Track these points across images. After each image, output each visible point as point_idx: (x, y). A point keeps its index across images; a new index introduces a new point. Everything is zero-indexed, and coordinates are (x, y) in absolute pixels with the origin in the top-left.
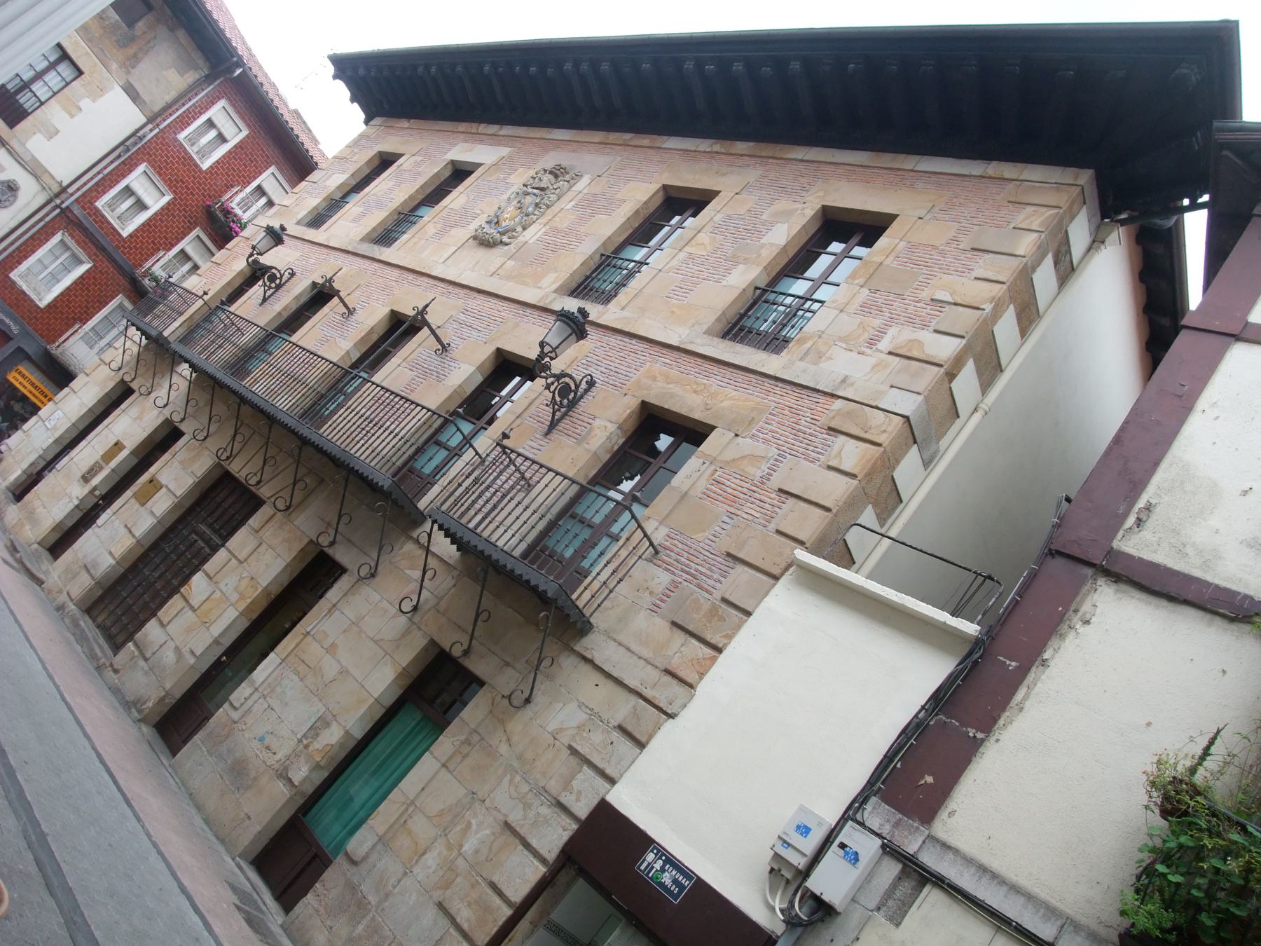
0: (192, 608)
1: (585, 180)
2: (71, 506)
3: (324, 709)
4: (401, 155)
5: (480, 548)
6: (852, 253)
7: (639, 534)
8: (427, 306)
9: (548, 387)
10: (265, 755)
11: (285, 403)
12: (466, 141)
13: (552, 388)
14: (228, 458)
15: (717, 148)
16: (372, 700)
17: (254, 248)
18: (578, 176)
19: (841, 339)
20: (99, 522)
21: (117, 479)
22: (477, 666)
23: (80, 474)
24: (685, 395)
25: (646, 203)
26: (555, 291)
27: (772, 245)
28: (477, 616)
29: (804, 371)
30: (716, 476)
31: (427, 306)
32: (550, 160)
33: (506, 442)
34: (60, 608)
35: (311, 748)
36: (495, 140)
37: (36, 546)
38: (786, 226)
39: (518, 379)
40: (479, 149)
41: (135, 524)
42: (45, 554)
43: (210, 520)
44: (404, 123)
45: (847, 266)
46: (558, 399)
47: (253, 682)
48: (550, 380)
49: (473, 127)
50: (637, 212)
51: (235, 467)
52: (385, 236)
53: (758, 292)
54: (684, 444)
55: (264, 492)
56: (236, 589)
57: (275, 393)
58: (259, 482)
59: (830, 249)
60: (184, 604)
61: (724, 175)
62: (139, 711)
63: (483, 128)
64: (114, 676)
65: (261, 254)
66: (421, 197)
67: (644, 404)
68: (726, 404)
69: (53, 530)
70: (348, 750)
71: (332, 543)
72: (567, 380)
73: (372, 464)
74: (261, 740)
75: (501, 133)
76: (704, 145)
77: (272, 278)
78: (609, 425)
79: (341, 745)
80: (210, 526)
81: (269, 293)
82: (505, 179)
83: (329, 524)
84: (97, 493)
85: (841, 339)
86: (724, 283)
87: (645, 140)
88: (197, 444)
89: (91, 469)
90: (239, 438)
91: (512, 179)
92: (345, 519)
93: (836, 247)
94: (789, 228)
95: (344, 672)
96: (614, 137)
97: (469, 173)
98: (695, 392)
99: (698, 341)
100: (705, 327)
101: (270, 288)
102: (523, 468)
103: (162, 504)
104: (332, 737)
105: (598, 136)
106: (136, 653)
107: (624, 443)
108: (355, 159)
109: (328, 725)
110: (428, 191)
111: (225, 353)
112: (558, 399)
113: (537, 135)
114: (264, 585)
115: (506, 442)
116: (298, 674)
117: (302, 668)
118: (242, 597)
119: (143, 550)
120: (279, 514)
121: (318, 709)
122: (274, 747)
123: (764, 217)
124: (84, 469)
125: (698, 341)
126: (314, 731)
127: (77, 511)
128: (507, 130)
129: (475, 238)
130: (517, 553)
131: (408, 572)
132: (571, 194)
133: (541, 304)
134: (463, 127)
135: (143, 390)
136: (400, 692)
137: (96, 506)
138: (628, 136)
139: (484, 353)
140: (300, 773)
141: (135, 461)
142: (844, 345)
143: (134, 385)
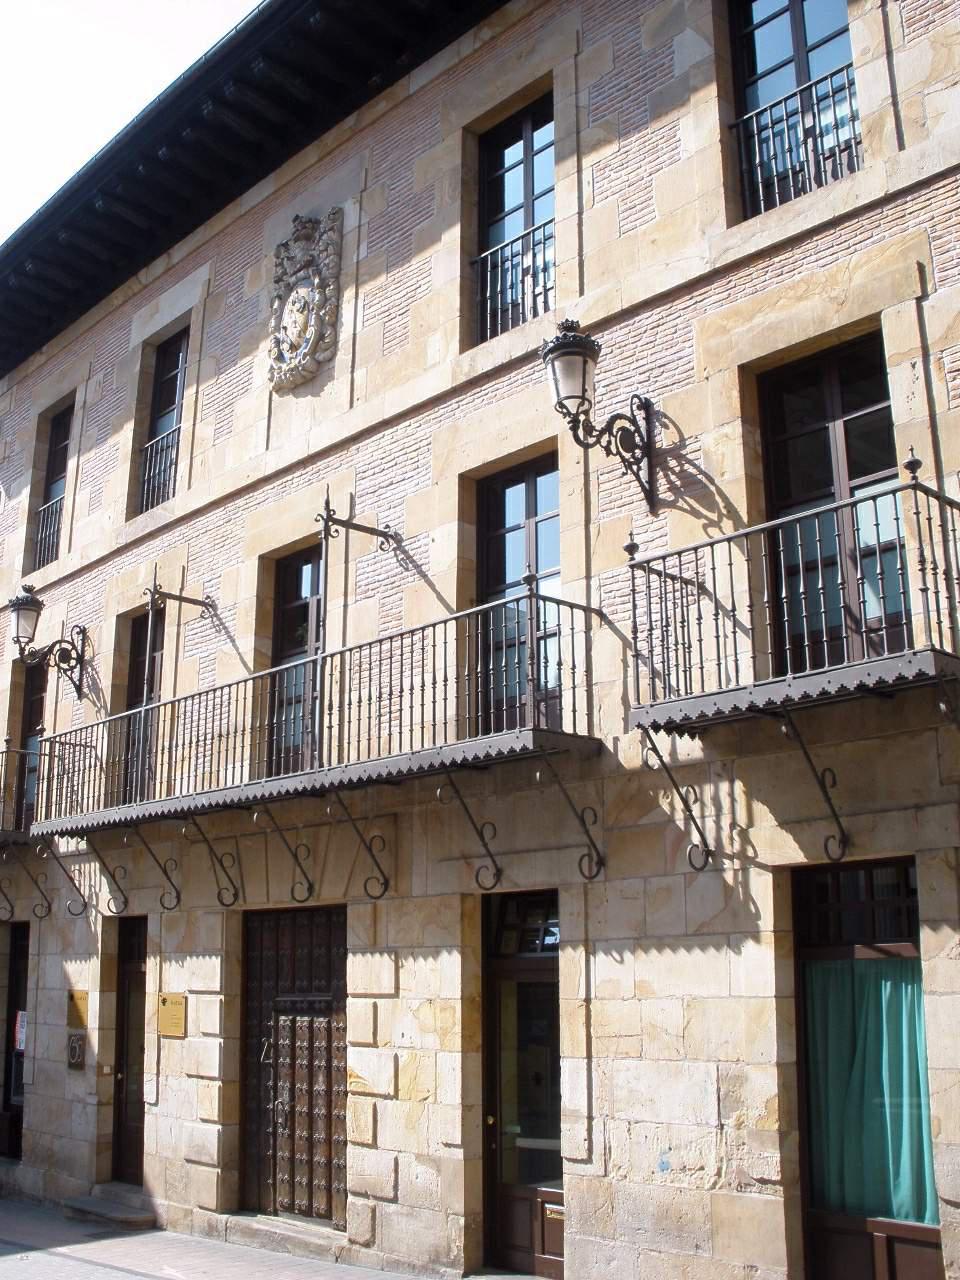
0: (386, 1097)
1: (351, 210)
2: (92, 1110)
3: (713, 1067)
4: (73, 394)
5: (761, 703)
6: (537, 147)
7: (565, 609)
8: (327, 503)
9: (608, 452)
10: (686, 1181)
11: (236, 776)
12: (139, 307)
13: (613, 449)
14: (236, 896)
15: (486, 33)
16: (774, 999)
17: (18, 641)
18: (338, 214)
19: (926, 83)
20: (149, 1094)
21: (113, 1034)
22: (882, 843)
23: (63, 1067)
24: (796, 309)
25: (463, 165)
26: (462, 351)
27: (697, 66)
28: (295, 856)
29: (923, 156)
30: (948, 367)
31: (327, 503)
32: (279, 227)
33: (639, 557)
34: (211, 1230)
35: (751, 1123)
36: (176, 274)
37: (97, 1189)
38: (689, 32)
39: (307, 570)
40: (167, 298)
41: (198, 1064)
42: (120, 1188)
43: (285, 983)
44: (38, 359)
45: (544, 162)
46: (627, 456)
47: (575, 1114)
48: (604, 442)
49: (132, 285)
50: (464, 183)
51: (256, 900)
52: (147, 490)
53: (734, 130)
54: (540, 480)
55: (328, 895)
56: (423, 1030)
57: (213, 775)
58: (311, 888)
59: (508, 163)
60: (371, 1100)
61: (532, 51)
62: (452, 1264)
63: (145, 276)
64: (371, 1251)
65: (31, 640)
66: (147, 412)
67: (742, 368)
68: (858, 278)
69: (98, 1154)
70: (795, 1084)
71: (499, 874)
72: (619, 424)
73: (406, 749)
74: (664, 1167)
75: (175, 260)
76: (466, 45)
77: (65, 656)
78: (727, 429)
79: (783, 1086)
80: (291, 990)
81: (76, 675)
82: (239, 300)
83: (466, 857)
84: (107, 1070)
85: (926, 83)
86: (684, 156)
87: (380, 105)
88: (175, 913)
89: (72, 1050)
90: (227, 862)
91: (248, 291)
92: (488, 833)
93: (514, 153)
94: (697, 30)
95: (690, 1003)
96: (330, 138)
97: (184, 333)
98: (800, 299)
99: (731, 242)
100: (722, 219)
101: (72, 669)
102: (675, 571)
103: (207, 1014)
104: (764, 1086)
105: (310, 154)
106: (371, 1203)
107: (763, 435)
108: (17, 448)
109: (740, 1079)
110: (149, 398)
111: (93, 785)
112: (627, 456)
113: (228, 221)
114: (458, 995)
115: (639, 557)
116: (627, 1056)
117: (625, 1045)
118: (444, 1033)
119: (237, 1085)
120: (380, 902)
121: (703, 1075)
122: (691, 1158)
123: (646, 48)
124: (64, 1057)
125: (731, 242)
126: (726, 1101)
127: (104, 1109)
128: (179, 251)
129: (280, 389)
130: (246, 780)
131: (644, 821)
132: (350, 240)
133: (462, 379)
134: (117, 297)
135: (40, 911)
136: (791, 962)
137: (119, 1084)
138: (350, 121)
139: (448, 499)
140: (769, 1161)
141: (113, 996)
142: (939, 86)
143: (20, 916)
